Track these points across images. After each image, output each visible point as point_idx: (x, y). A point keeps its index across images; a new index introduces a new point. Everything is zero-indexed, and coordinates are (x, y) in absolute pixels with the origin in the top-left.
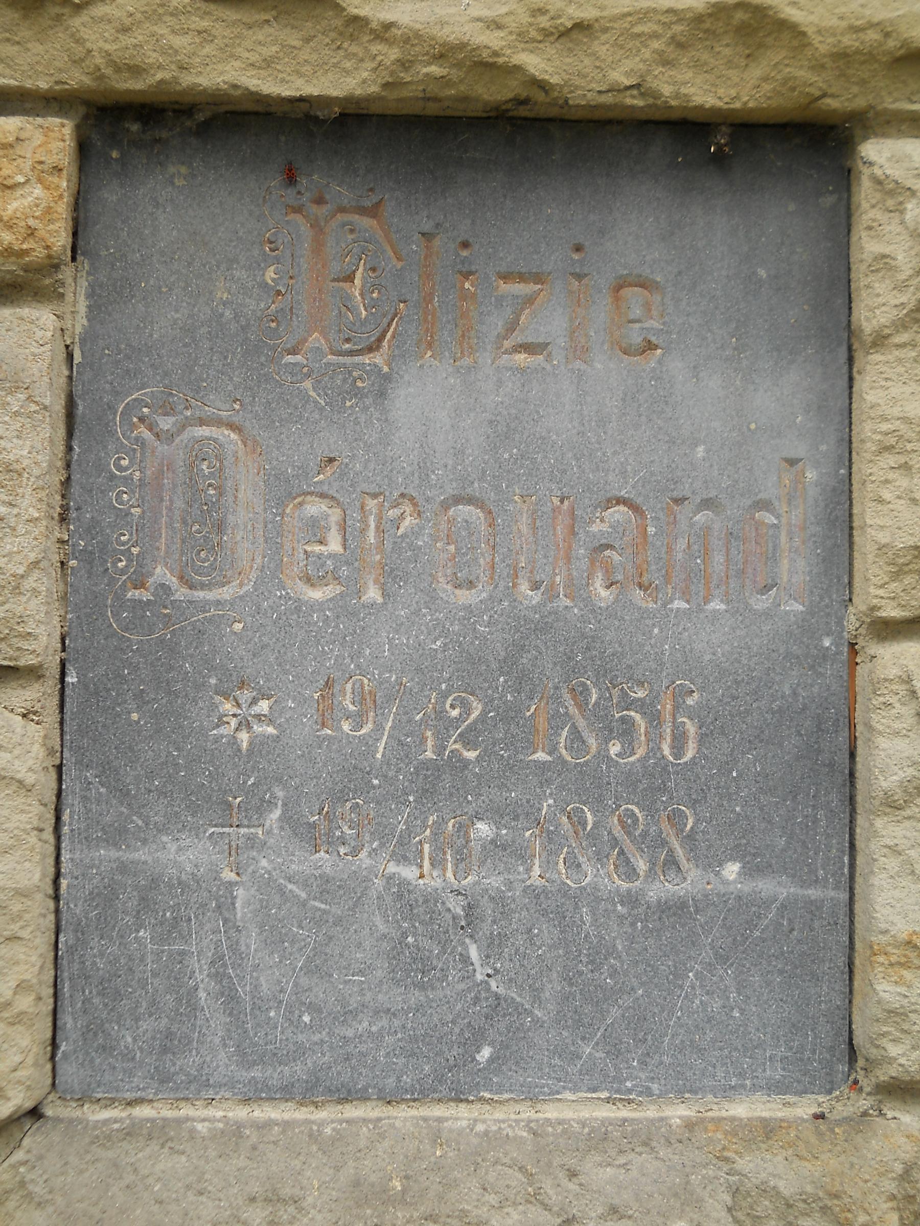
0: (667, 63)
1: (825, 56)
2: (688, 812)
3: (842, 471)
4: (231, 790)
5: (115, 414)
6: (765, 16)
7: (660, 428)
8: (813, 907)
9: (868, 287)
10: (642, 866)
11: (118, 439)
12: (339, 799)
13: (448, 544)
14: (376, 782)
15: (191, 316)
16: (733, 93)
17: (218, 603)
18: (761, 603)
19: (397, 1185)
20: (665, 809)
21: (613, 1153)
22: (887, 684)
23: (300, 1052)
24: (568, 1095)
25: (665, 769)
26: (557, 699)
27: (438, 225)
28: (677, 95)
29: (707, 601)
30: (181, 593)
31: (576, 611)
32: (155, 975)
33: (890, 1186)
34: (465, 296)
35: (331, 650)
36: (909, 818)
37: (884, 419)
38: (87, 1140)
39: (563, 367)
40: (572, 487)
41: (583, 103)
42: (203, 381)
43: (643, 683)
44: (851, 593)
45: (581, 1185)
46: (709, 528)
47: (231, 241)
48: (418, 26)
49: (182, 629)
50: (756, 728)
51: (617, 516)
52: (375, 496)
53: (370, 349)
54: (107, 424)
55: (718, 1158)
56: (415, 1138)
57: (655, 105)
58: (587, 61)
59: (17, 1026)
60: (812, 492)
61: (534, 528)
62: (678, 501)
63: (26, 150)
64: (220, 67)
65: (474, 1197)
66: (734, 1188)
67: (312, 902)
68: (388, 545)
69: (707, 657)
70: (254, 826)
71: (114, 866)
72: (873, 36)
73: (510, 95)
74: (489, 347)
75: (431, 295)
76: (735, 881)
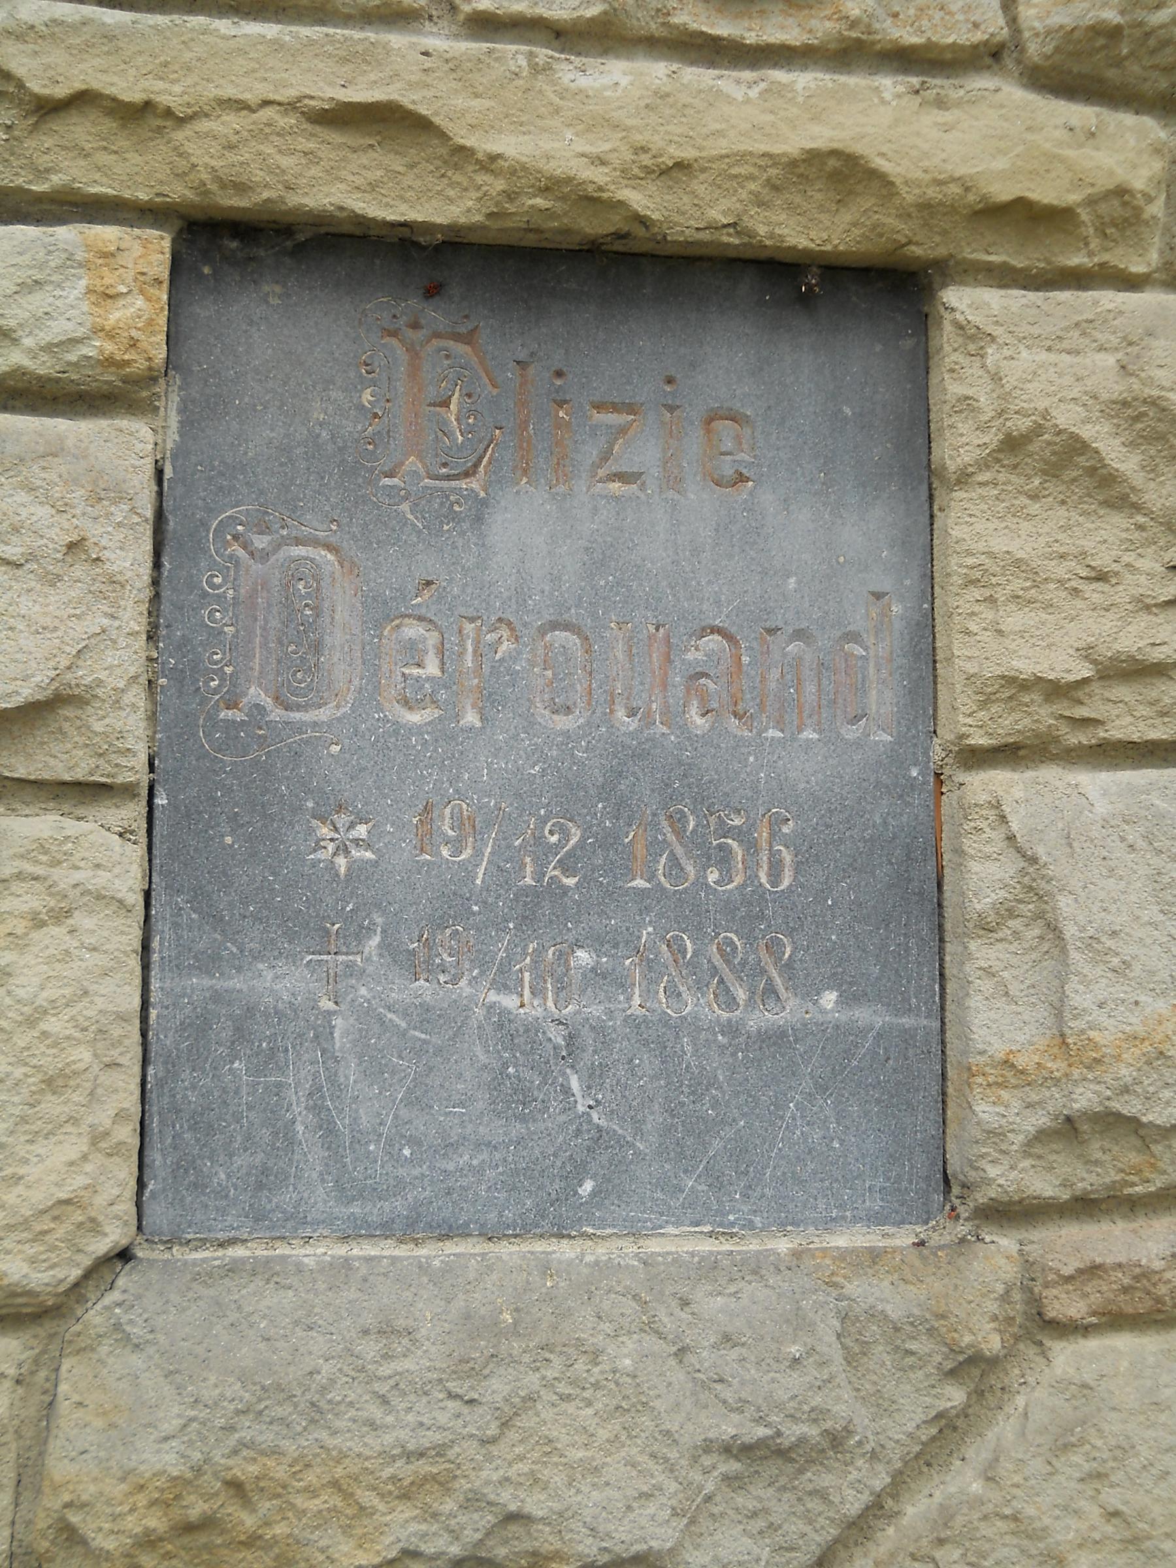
0: (761, 204)
1: (912, 205)
2: (785, 940)
3: (925, 606)
4: (329, 916)
5: (208, 531)
6: (857, 164)
7: (753, 559)
8: (907, 1036)
9: (951, 427)
10: (741, 995)
11: (211, 556)
12: (439, 925)
13: (545, 669)
14: (476, 908)
15: (287, 436)
16: (825, 236)
17: (315, 724)
18: (851, 733)
19: (508, 1317)
20: (764, 937)
21: (723, 1281)
22: (977, 809)
23: (400, 1186)
24: (671, 1230)
25: (762, 896)
26: (656, 826)
27: (532, 354)
28: (771, 236)
29: (800, 731)
30: (276, 714)
31: (673, 738)
32: (250, 1108)
33: (992, 1307)
34: (559, 424)
35: (430, 774)
36: (1001, 940)
37: (969, 553)
38: (189, 1277)
39: (657, 497)
40: (667, 615)
41: (682, 239)
42: (300, 500)
43: (739, 811)
44: (935, 724)
45: (693, 1314)
46: (800, 658)
47: (327, 362)
48: (524, 159)
49: (278, 750)
50: (849, 856)
51: (711, 645)
52: (472, 620)
53: (467, 474)
54: (199, 542)
55: (827, 1283)
56: (522, 1270)
57: (750, 244)
58: (686, 199)
59: (115, 1157)
60: (898, 625)
61: (630, 656)
62: (771, 631)
63: (125, 259)
64: (325, 189)
65: (589, 1325)
66: (843, 1313)
67: (412, 1032)
68: (486, 669)
69: (802, 786)
70: (353, 953)
71: (208, 995)
72: (955, 189)
73: (612, 230)
74: (584, 475)
75: (526, 423)
76: (832, 1011)
